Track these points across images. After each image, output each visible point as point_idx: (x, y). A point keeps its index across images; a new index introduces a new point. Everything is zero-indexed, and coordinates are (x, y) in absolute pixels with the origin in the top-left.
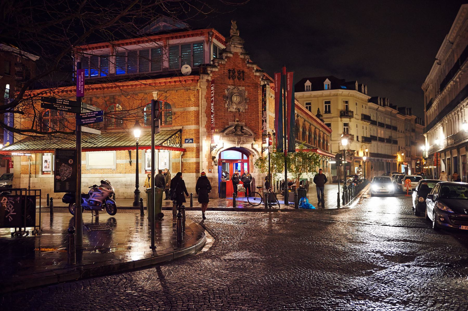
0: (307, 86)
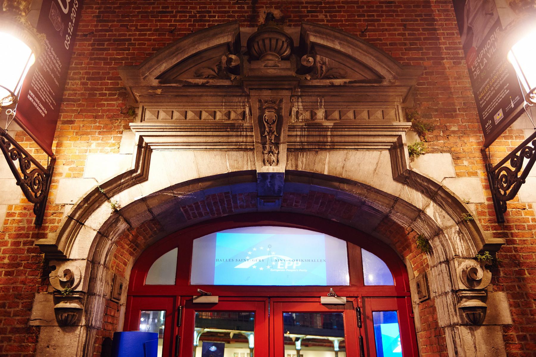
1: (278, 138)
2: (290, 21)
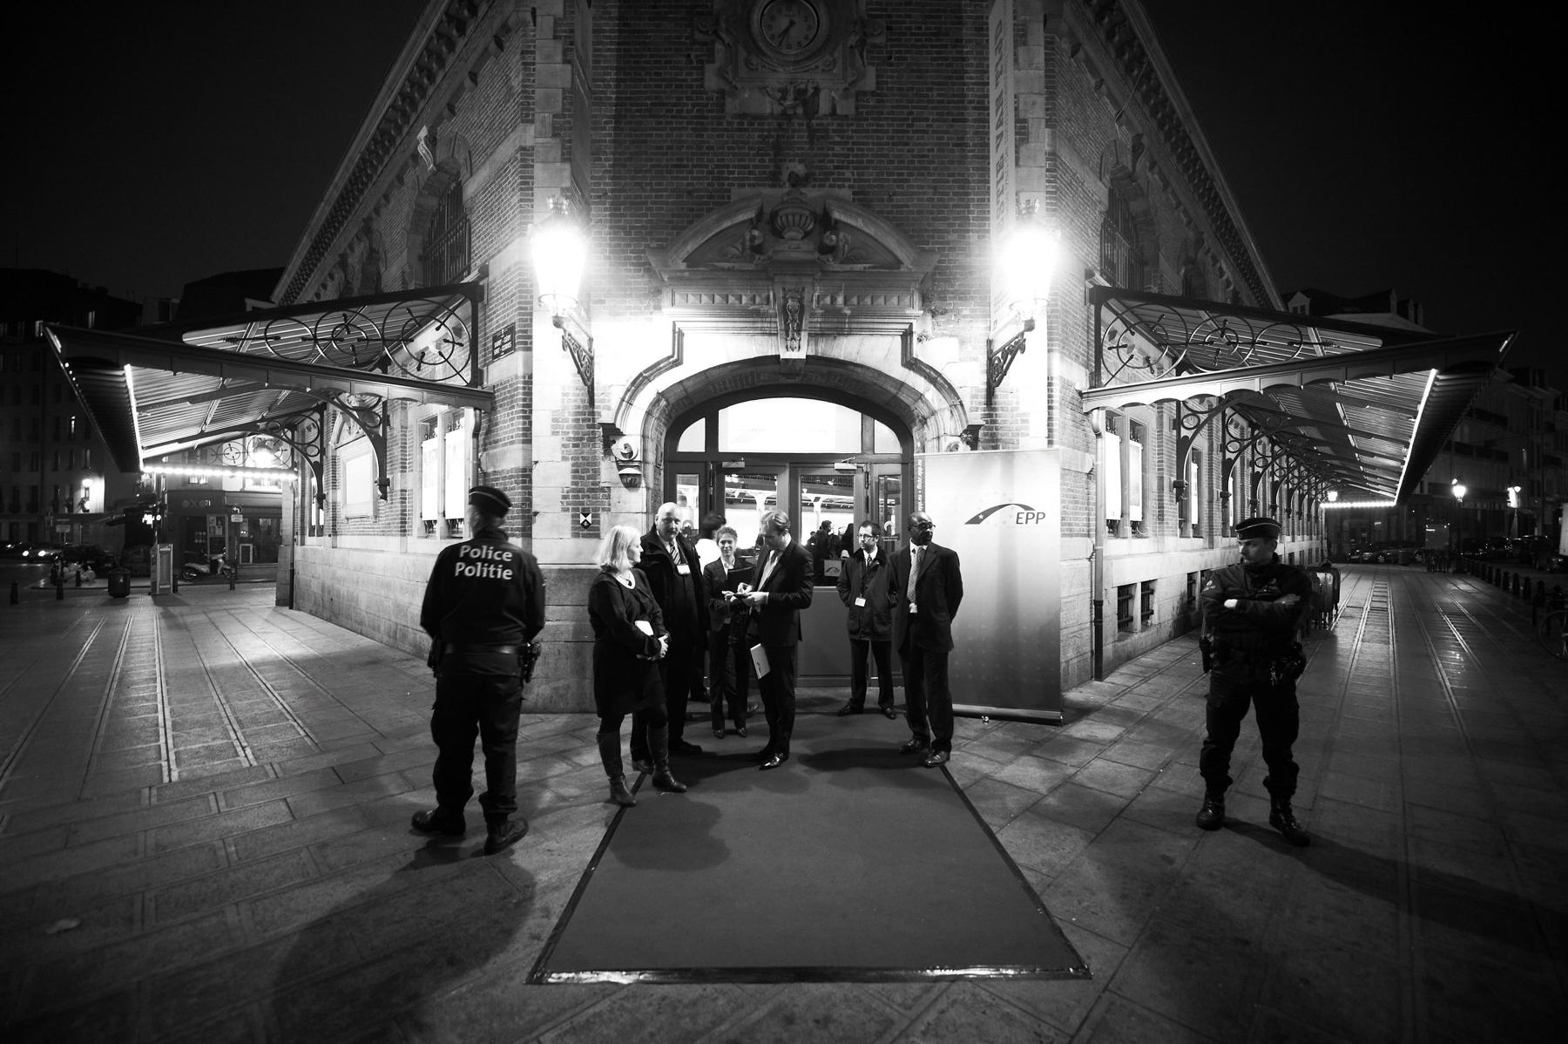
1: (800, 326)
2: (815, 180)
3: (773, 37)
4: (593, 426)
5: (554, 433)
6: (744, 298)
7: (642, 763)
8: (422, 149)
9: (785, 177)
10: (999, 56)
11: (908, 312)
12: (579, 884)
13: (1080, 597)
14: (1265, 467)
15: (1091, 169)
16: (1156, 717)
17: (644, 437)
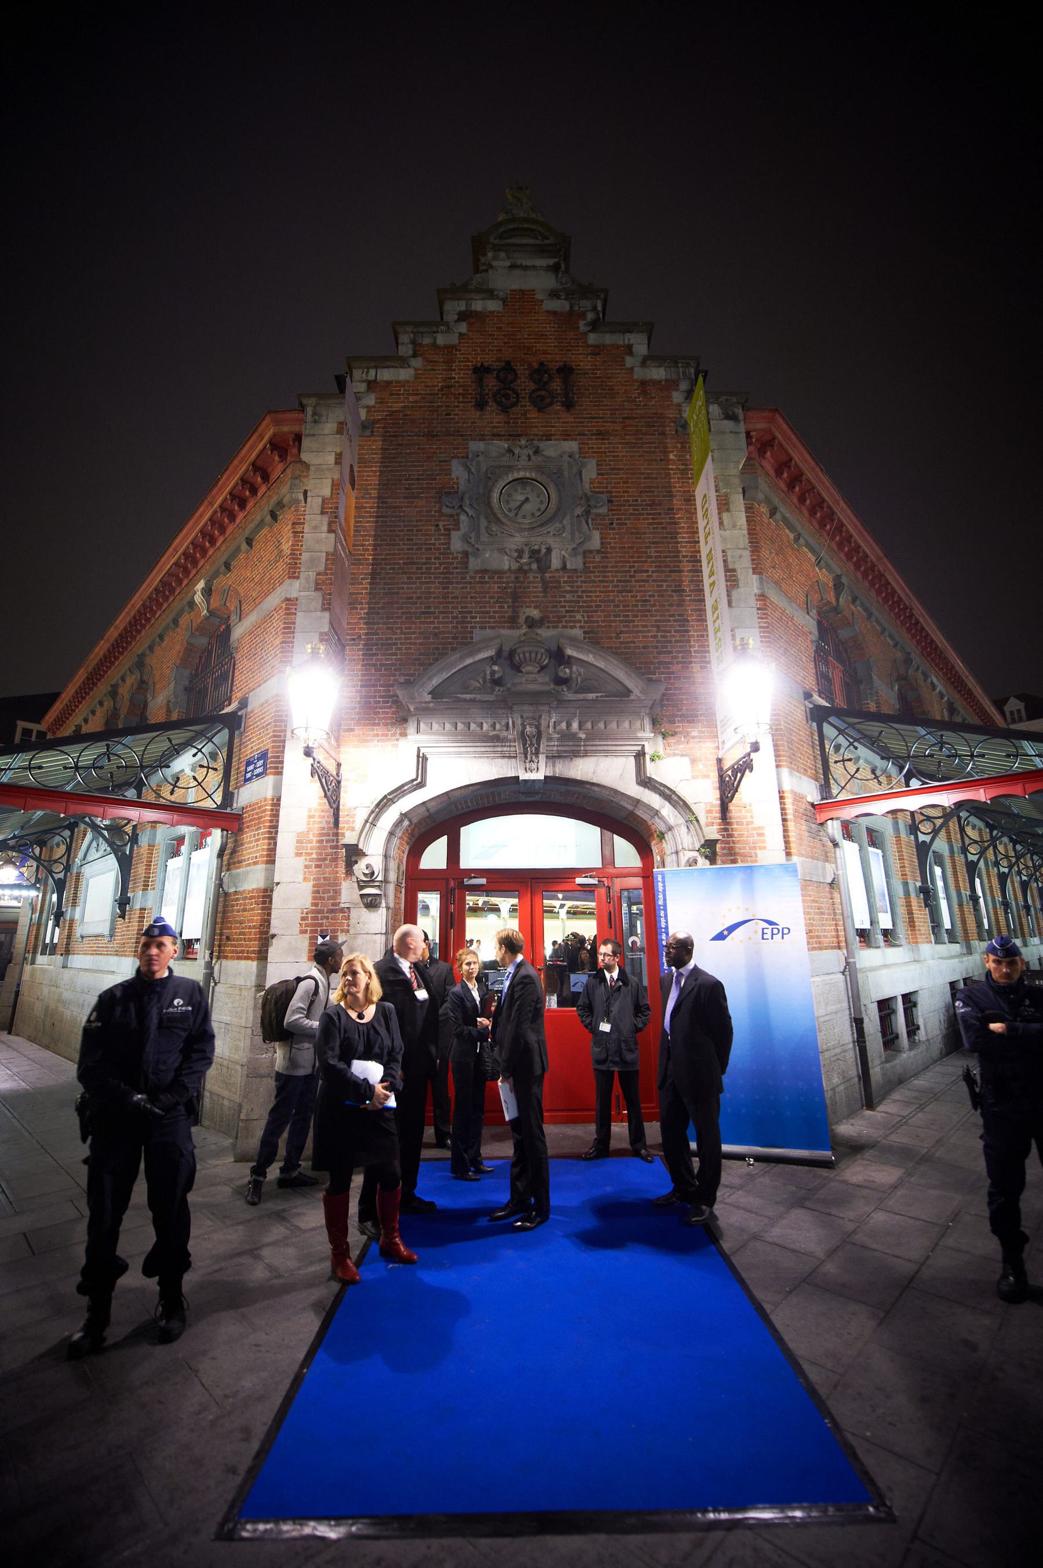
0: (1012, 713)
2: (549, 622)
3: (510, 510)
4: (336, 847)
5: (298, 855)
6: (485, 725)
7: (369, 1224)
8: (198, 598)
9: (522, 620)
10: (706, 521)
11: (640, 735)
12: (288, 1392)
13: (839, 1015)
14: (1010, 867)
15: (799, 606)
16: (937, 1155)
17: (386, 856)
